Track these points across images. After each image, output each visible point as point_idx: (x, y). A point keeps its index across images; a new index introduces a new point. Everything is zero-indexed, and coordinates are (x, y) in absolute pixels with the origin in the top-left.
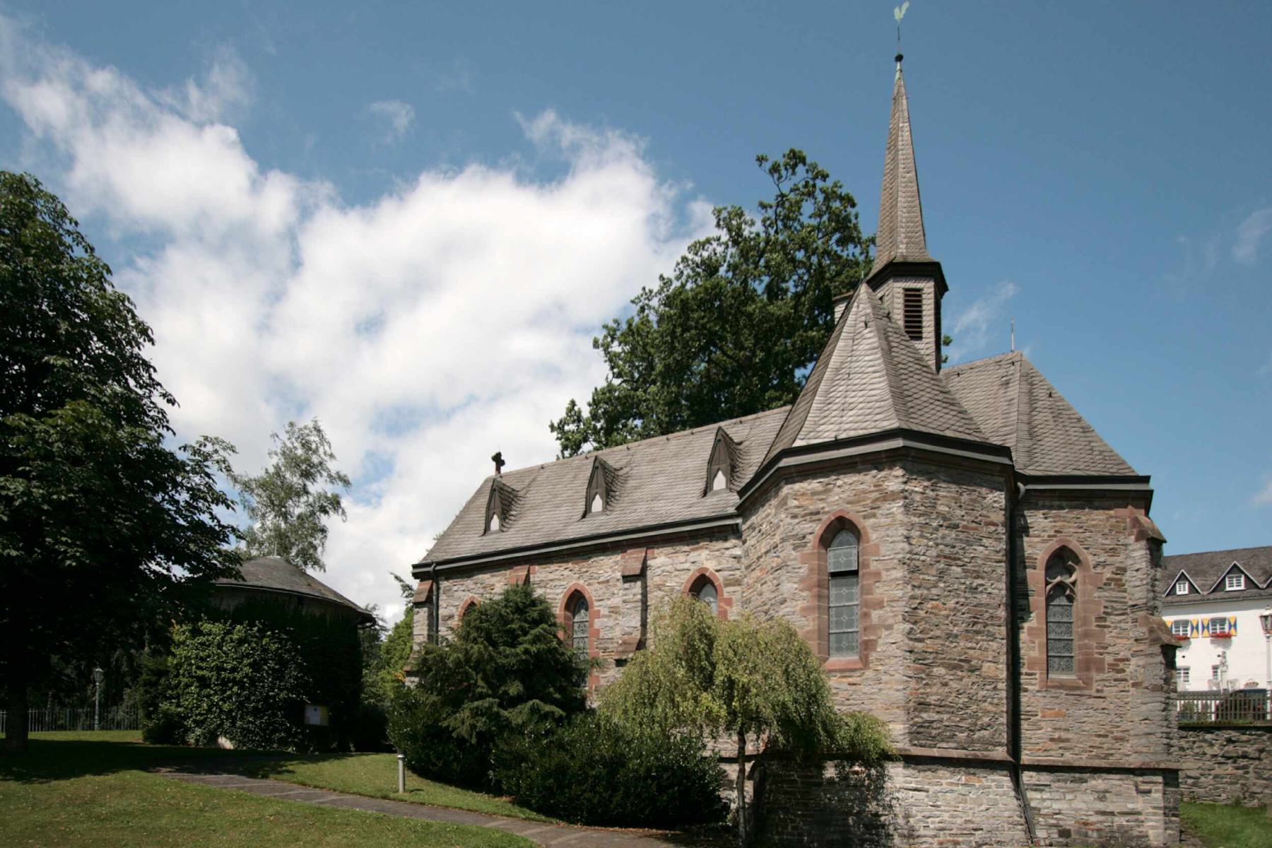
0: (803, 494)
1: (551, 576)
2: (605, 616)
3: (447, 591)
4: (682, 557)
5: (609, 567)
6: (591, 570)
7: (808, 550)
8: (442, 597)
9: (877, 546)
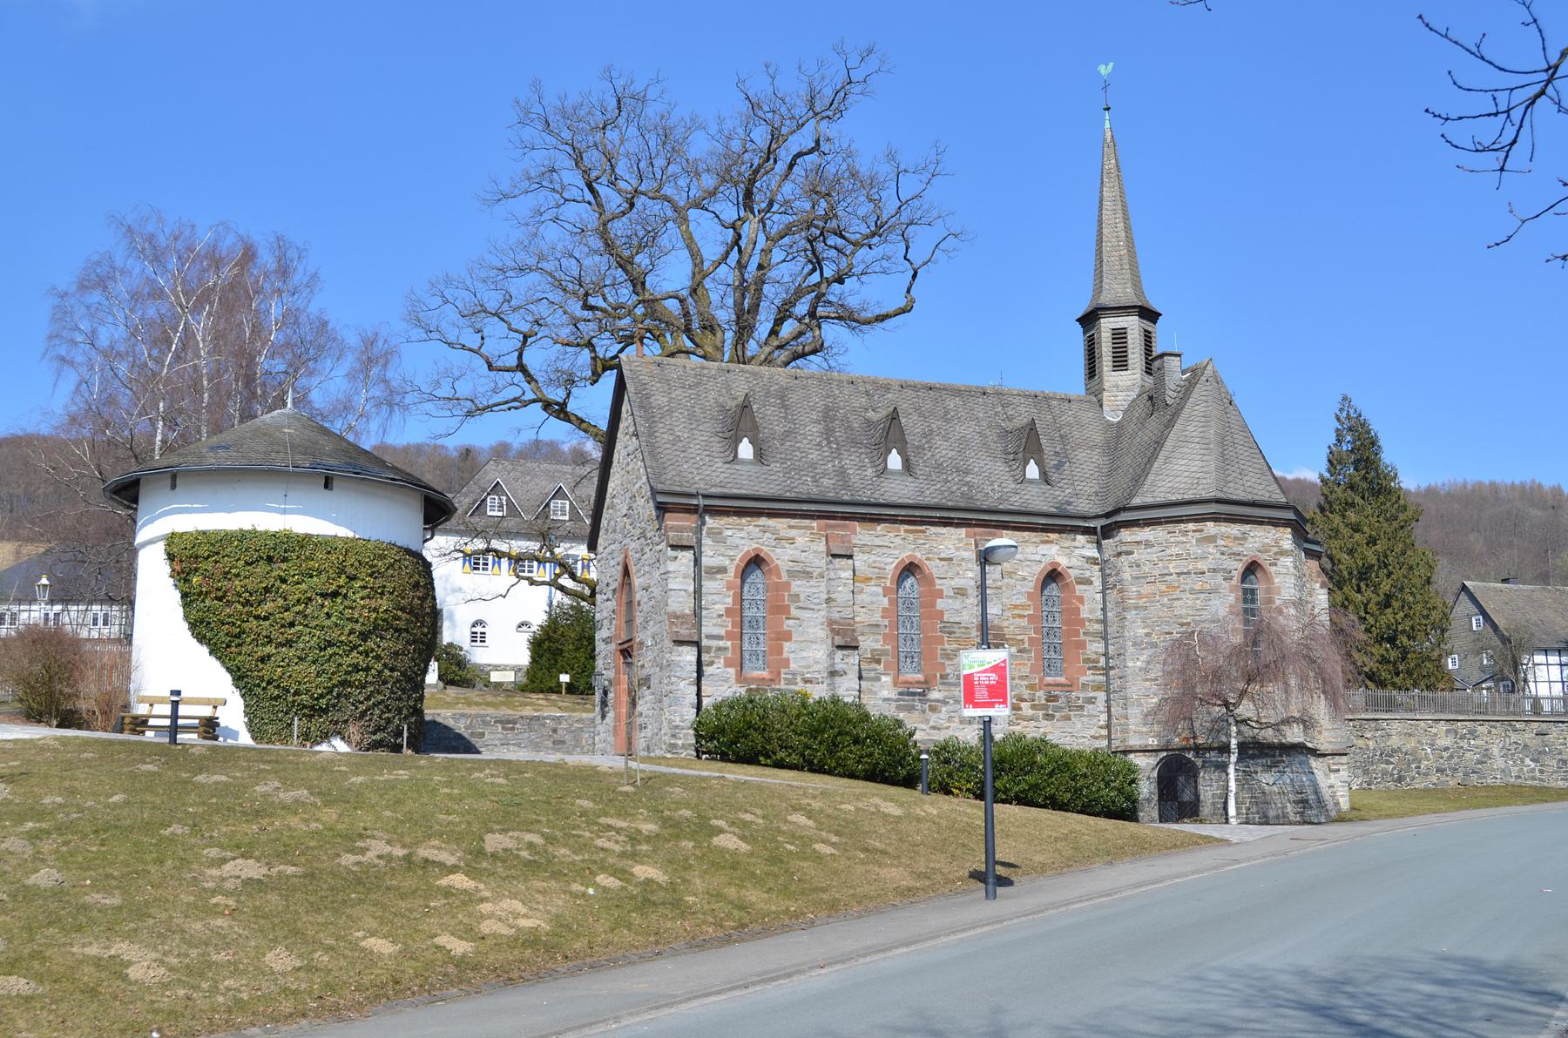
1: (878, 542)
3: (716, 535)
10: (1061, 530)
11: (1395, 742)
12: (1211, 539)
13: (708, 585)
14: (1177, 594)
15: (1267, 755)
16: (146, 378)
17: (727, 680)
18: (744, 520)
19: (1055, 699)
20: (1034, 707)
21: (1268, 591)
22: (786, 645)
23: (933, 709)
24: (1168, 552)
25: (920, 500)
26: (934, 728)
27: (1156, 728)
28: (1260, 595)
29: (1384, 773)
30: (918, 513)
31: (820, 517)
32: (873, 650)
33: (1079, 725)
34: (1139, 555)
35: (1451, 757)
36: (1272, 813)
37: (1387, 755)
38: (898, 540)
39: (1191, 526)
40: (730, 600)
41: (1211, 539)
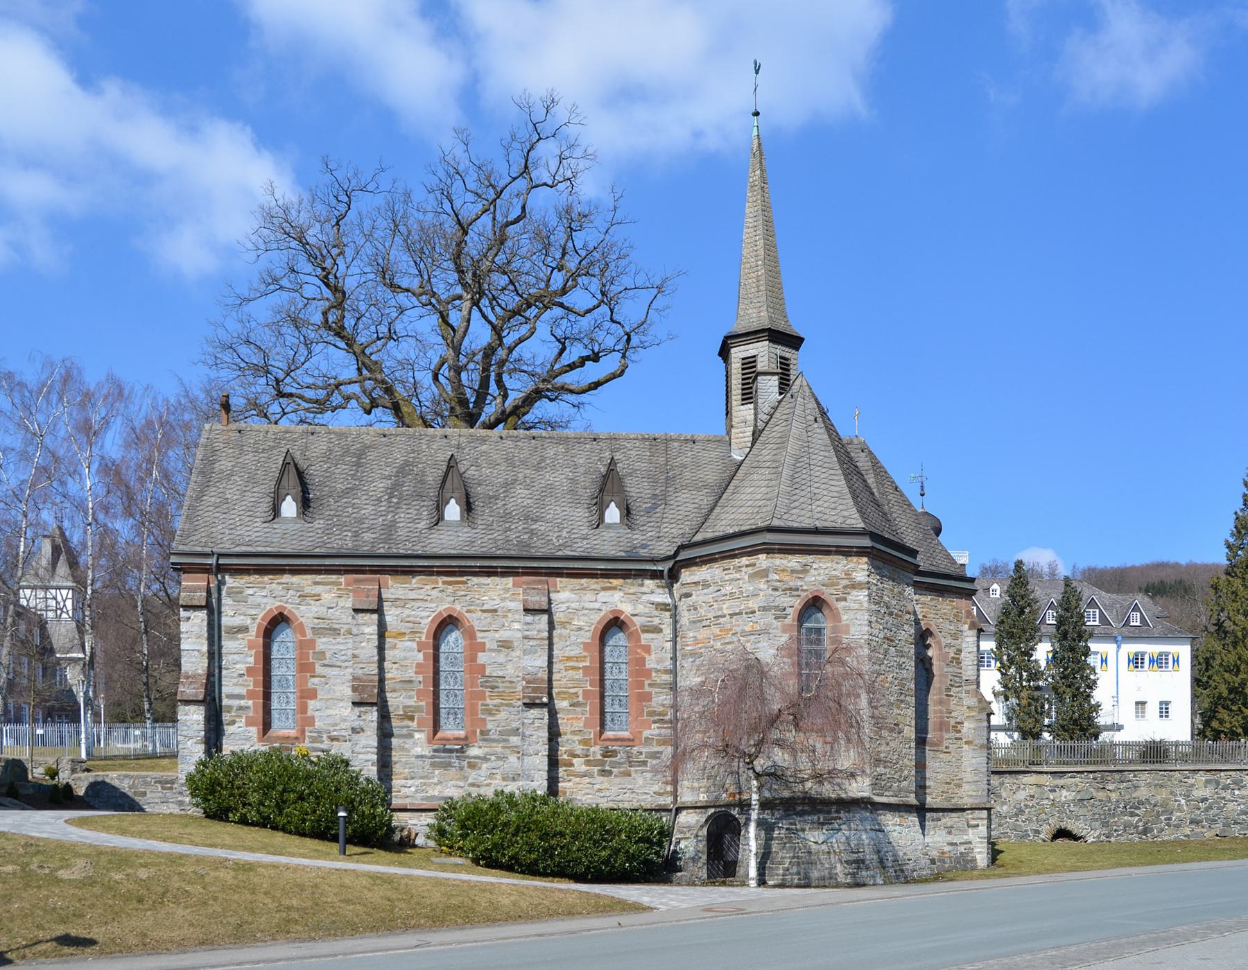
0: (783, 570)
1: (413, 595)
2: (492, 650)
3: (236, 593)
4: (589, 596)
5: (499, 594)
6: (471, 595)
7: (789, 621)
8: (226, 601)
9: (848, 626)
10: (626, 575)
11: (1143, 793)
12: (764, 574)
13: (228, 645)
15: (820, 812)
17: (248, 739)
18: (266, 578)
19: (614, 753)
20: (588, 763)
21: (835, 630)
22: (312, 704)
23: (472, 766)
24: (723, 591)
25: (467, 551)
26: (473, 785)
27: (704, 783)
28: (827, 633)
29: (1127, 826)
30: (454, 563)
31: (347, 572)
32: (405, 707)
33: (640, 781)
34: (698, 596)
35: (1207, 809)
36: (815, 874)
37: (1132, 807)
38: (435, 593)
39: (745, 560)
40: (251, 660)
41: (764, 574)
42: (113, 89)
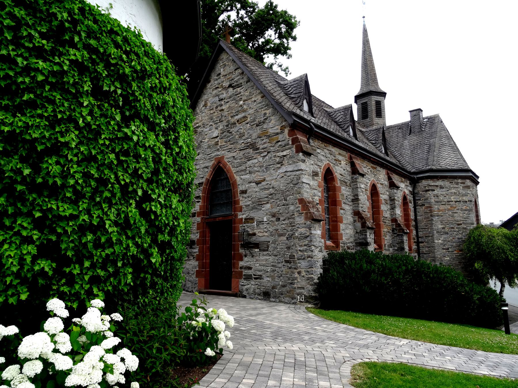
14: (455, 211)
16: (259, 17)
39: (460, 181)
42: (205, 91)
